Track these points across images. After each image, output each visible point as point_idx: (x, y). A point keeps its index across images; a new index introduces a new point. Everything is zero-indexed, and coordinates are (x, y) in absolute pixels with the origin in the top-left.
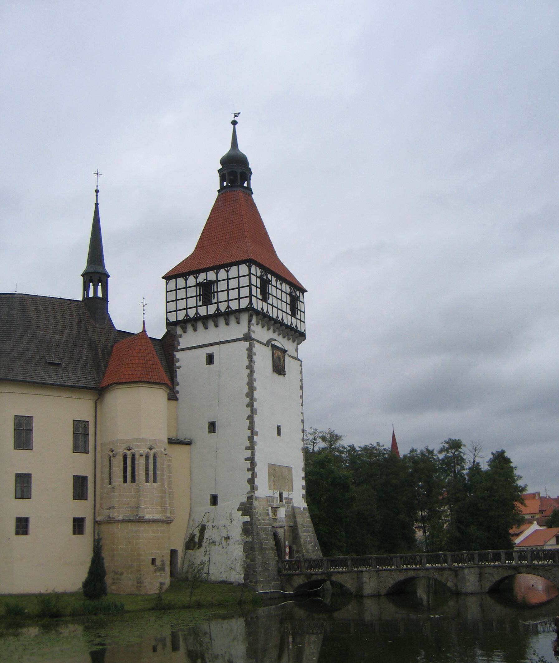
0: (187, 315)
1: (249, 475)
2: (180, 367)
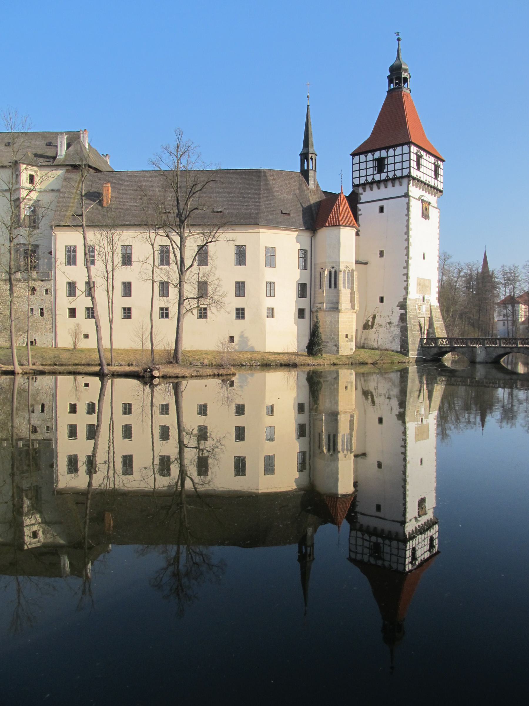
0: (366, 180)
2: (361, 215)
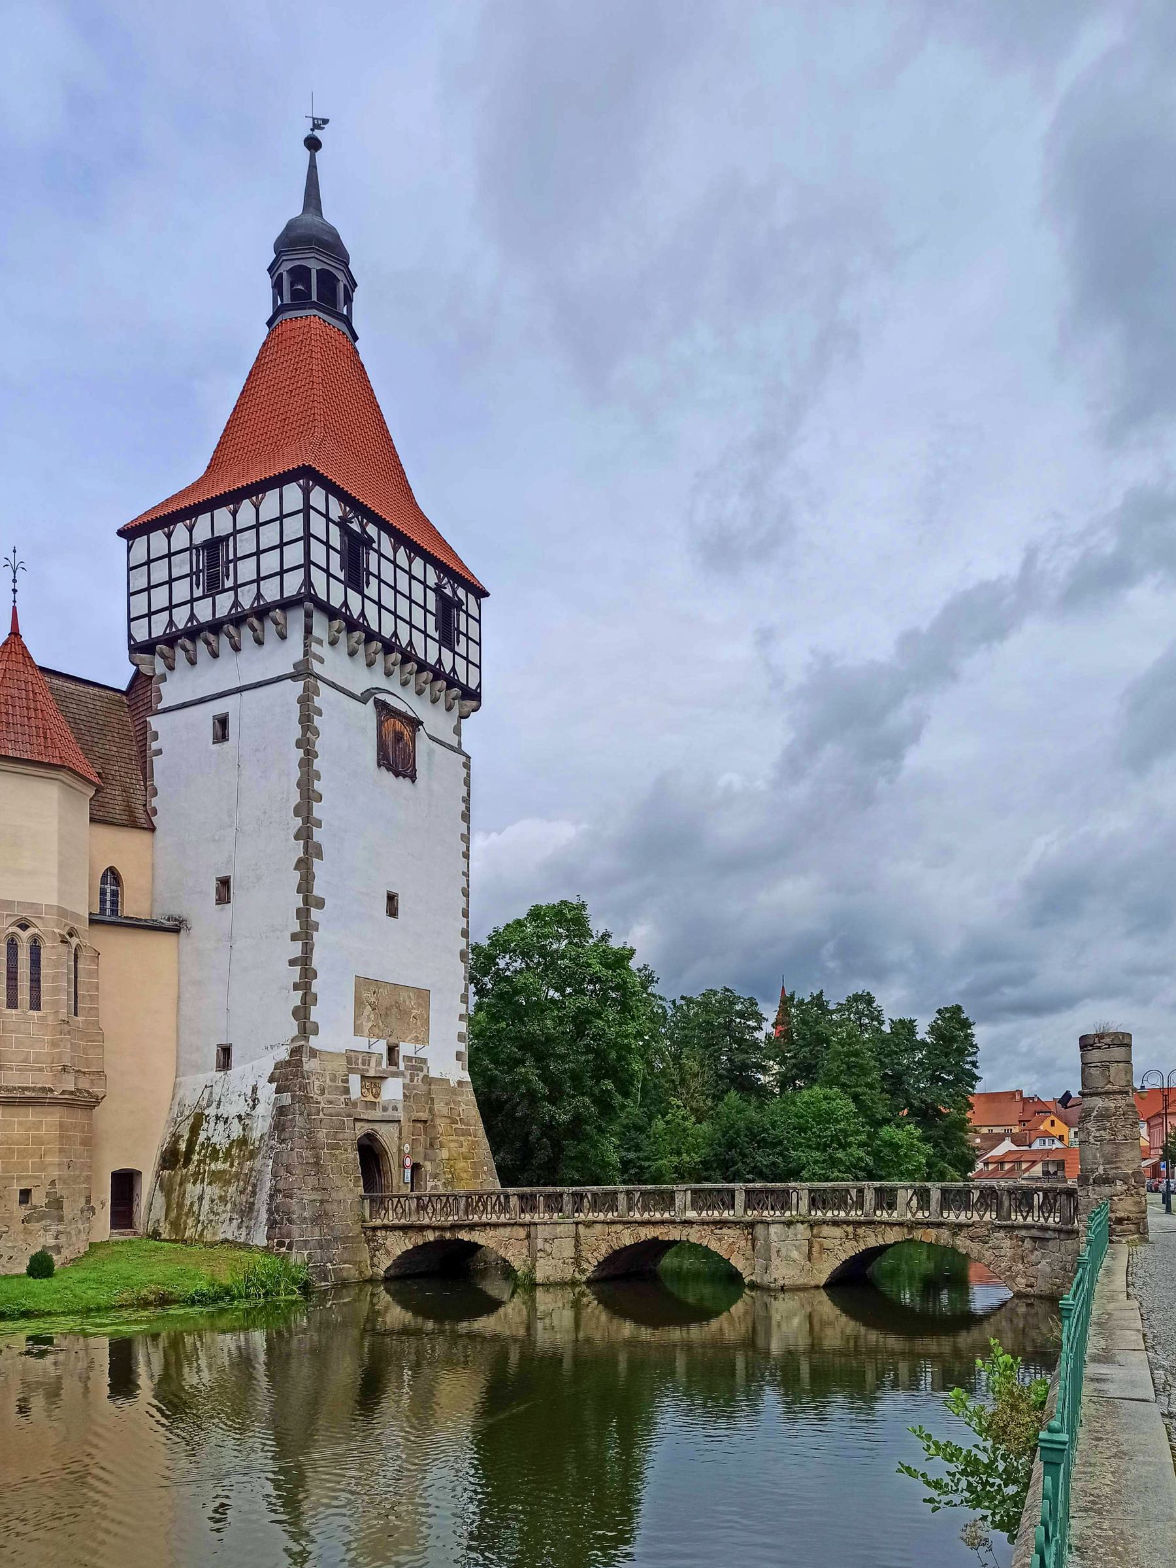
1: (296, 998)
2: (159, 752)
